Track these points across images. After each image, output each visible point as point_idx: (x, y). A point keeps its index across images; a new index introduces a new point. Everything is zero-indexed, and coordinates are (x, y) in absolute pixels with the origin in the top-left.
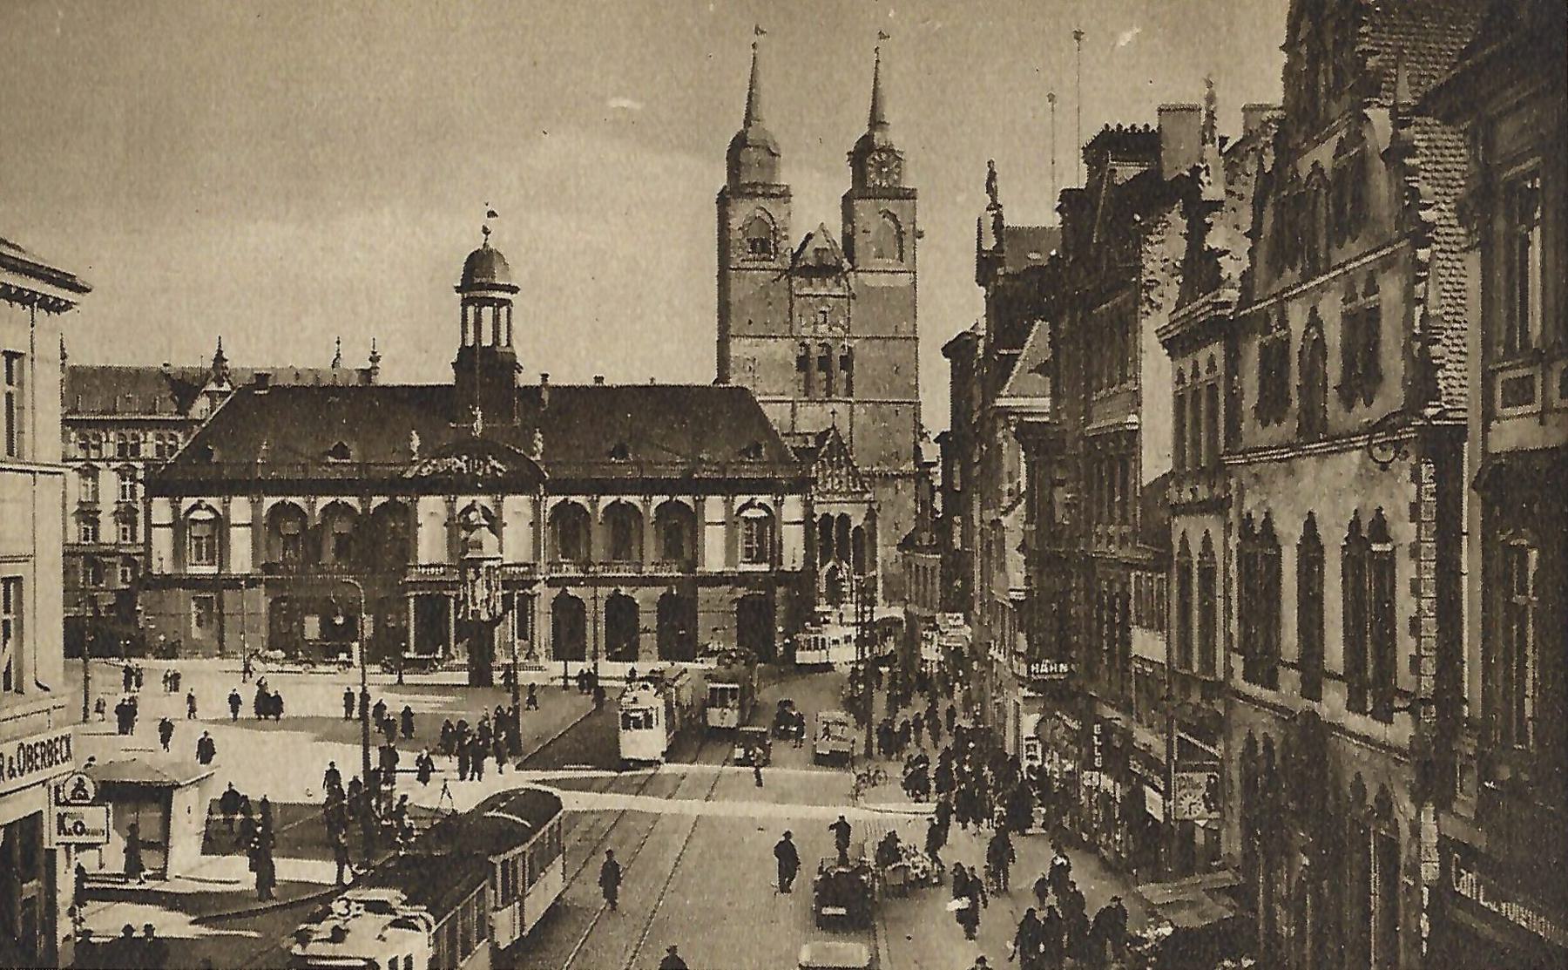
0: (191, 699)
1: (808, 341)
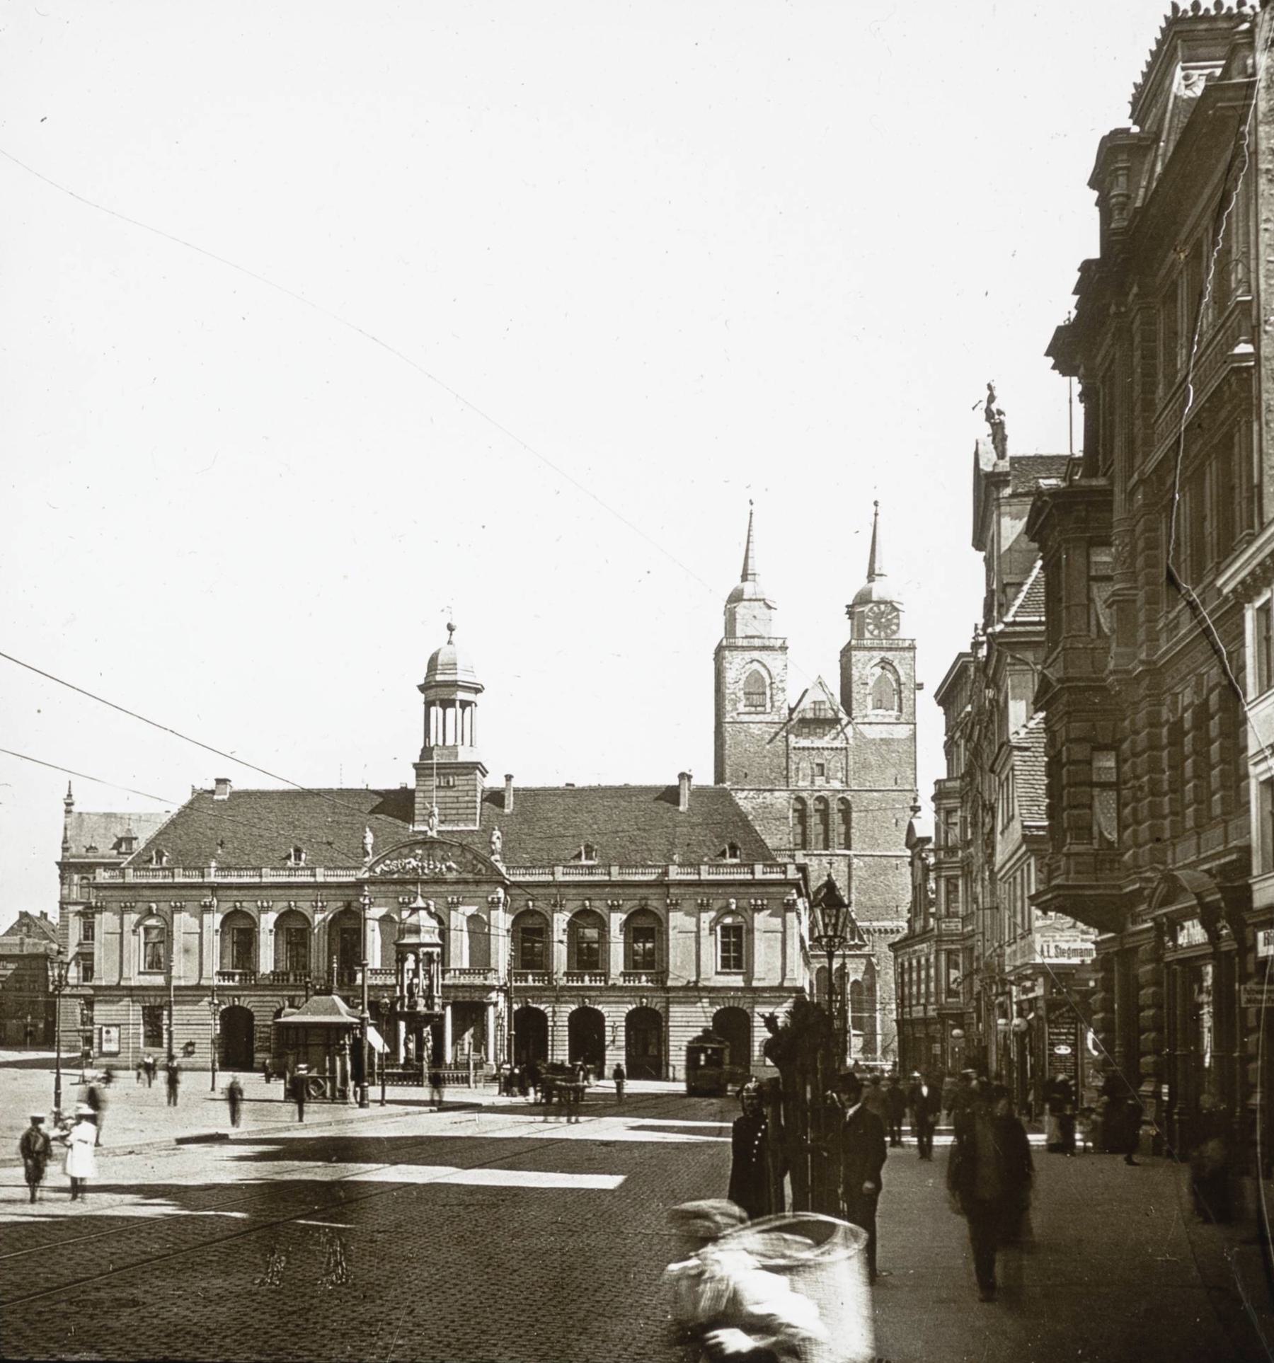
0: (80, 1140)
1: (804, 794)
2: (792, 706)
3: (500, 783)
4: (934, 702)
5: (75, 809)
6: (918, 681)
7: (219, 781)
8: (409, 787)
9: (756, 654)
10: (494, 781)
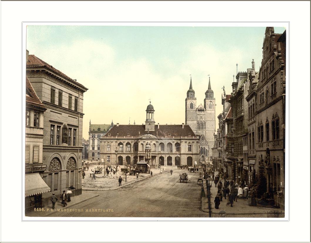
2: (197, 108)
3: (157, 124)
5: (91, 124)
7: (117, 124)
9: (192, 100)
10: (156, 124)
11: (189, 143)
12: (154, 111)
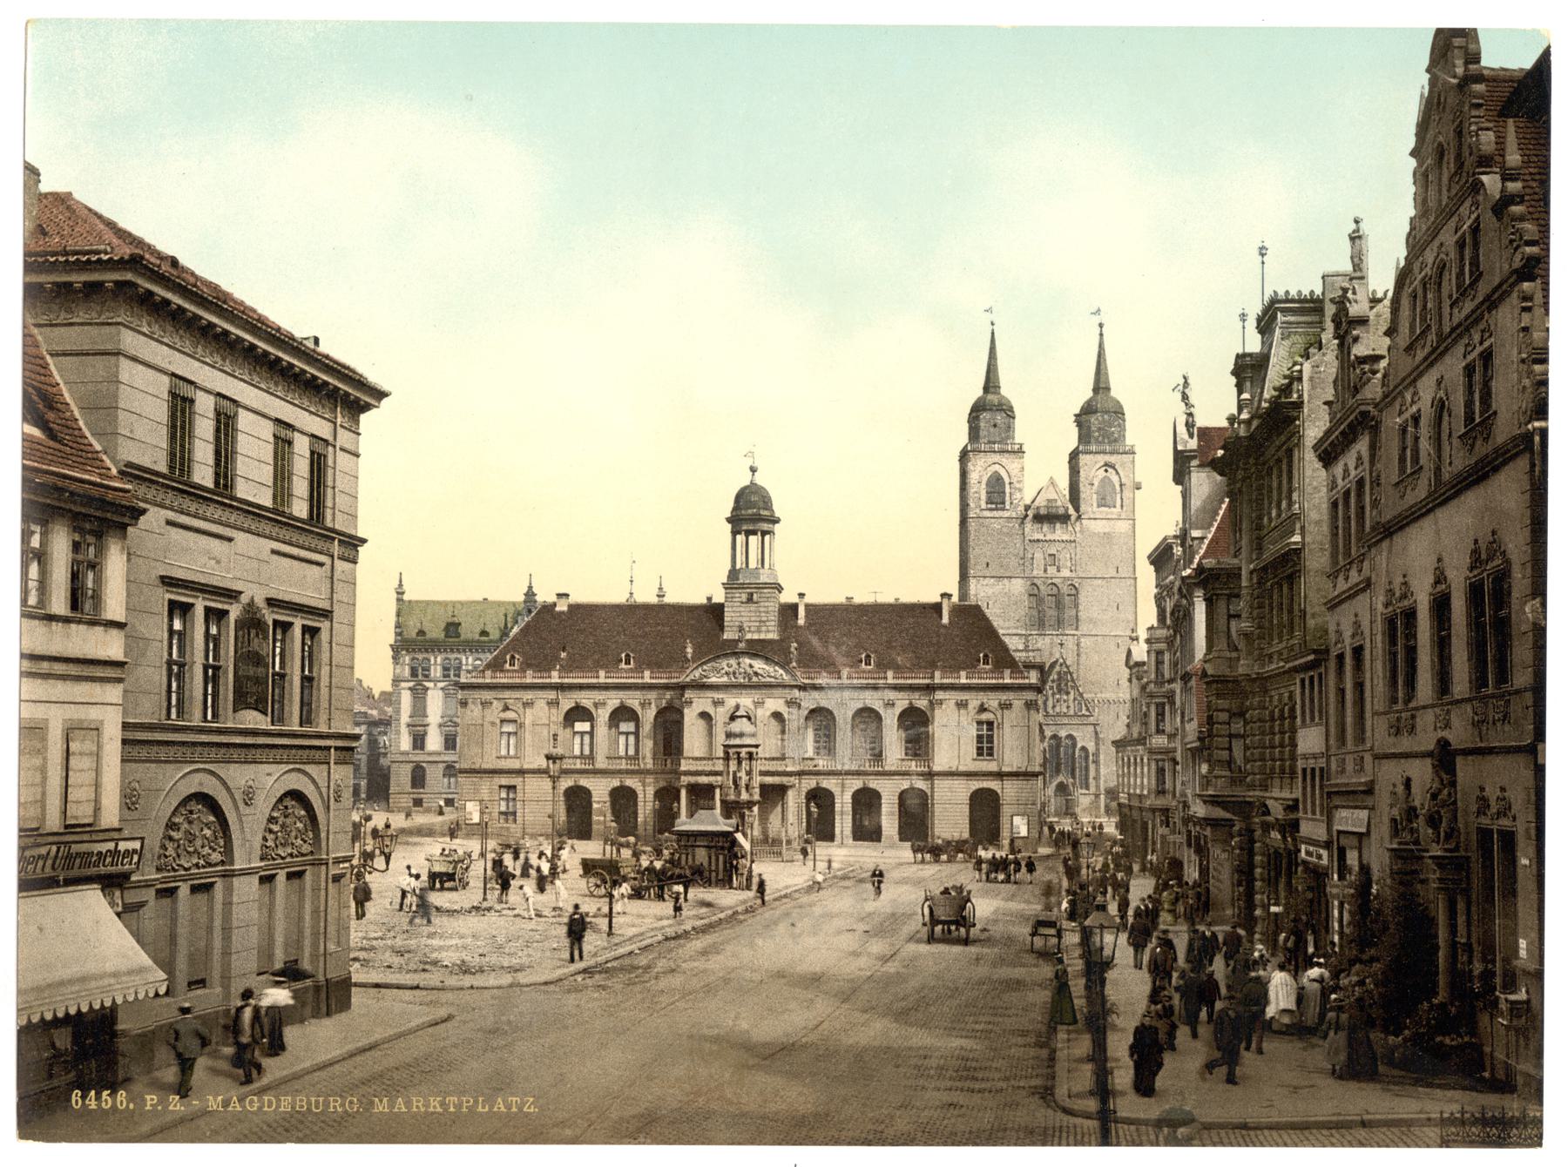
2: (1028, 502)
3: (795, 599)
4: (1147, 562)
6: (1137, 479)
8: (715, 600)
10: (788, 597)
11: (982, 709)
12: (777, 521)
